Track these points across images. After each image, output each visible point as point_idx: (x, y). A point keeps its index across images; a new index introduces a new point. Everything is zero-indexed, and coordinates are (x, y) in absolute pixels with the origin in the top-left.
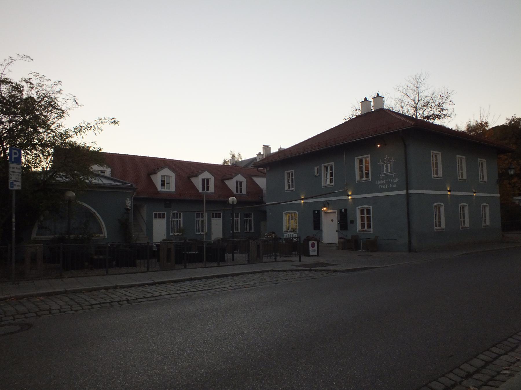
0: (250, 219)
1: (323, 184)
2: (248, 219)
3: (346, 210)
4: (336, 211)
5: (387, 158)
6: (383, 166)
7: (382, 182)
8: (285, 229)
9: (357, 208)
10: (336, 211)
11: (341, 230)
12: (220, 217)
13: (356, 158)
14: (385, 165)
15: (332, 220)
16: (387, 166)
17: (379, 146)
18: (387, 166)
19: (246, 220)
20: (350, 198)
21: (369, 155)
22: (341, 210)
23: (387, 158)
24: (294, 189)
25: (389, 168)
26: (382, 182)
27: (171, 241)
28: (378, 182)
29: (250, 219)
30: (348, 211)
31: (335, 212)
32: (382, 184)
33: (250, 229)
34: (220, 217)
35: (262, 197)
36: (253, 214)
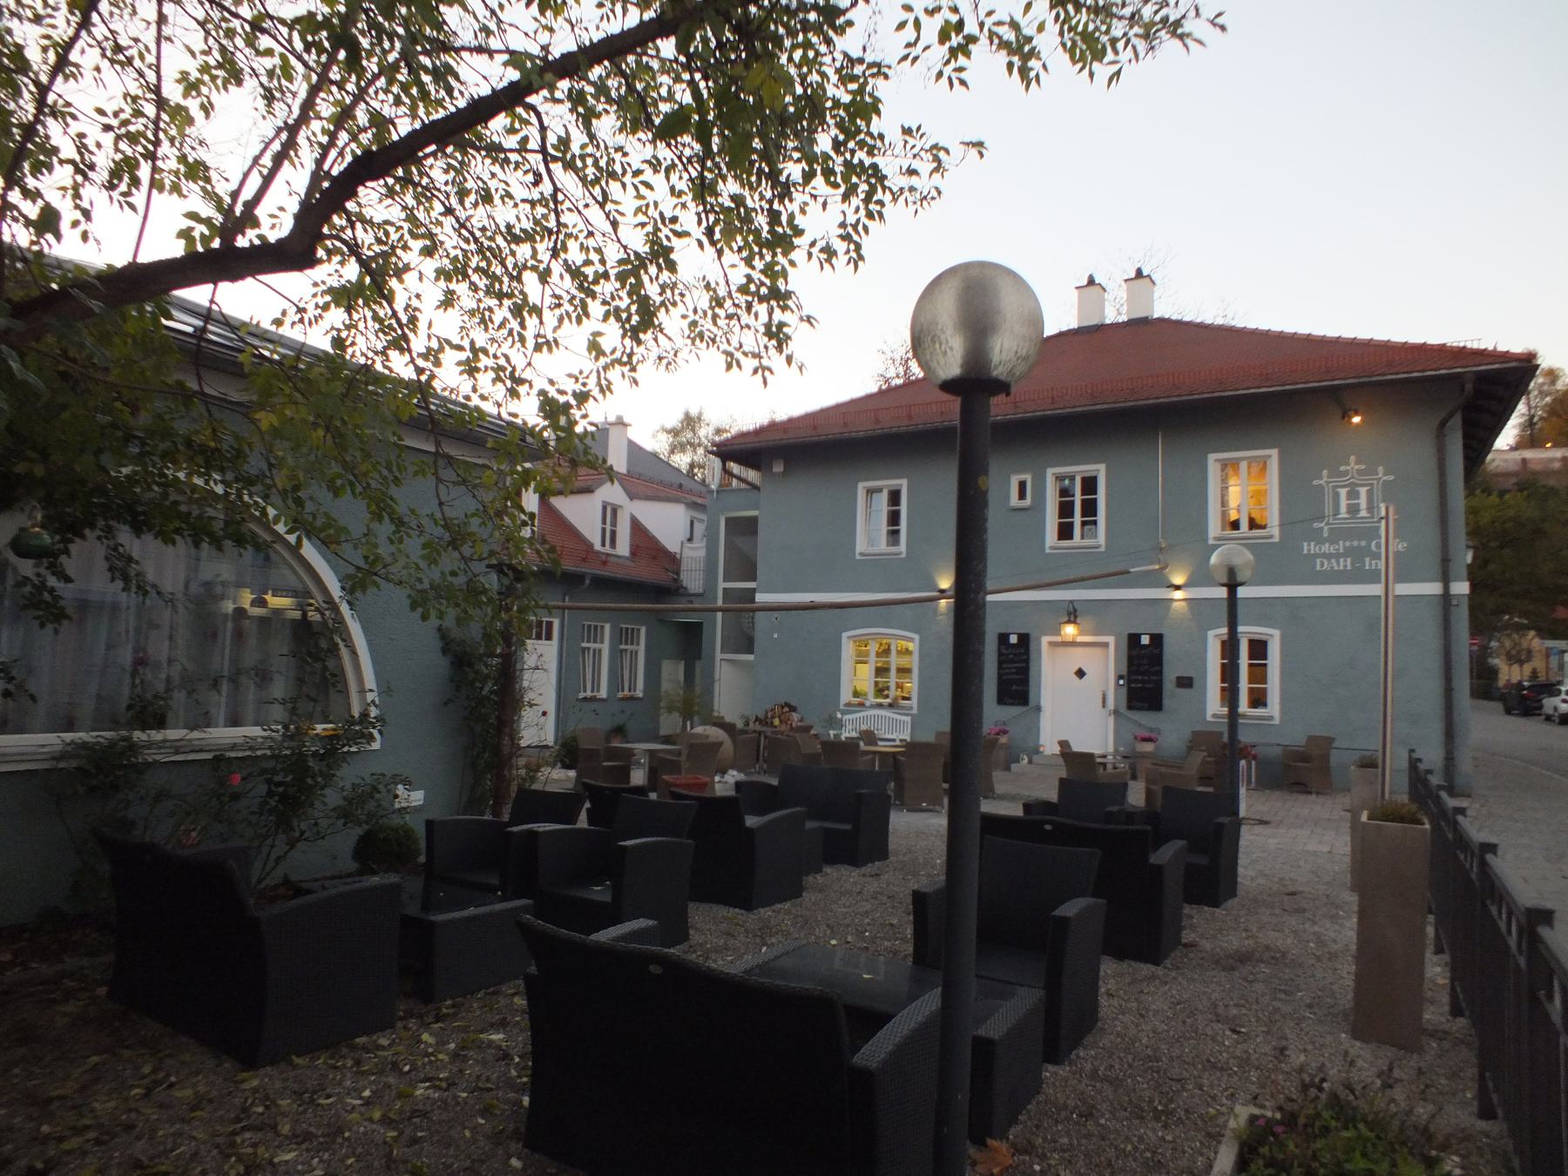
0: (597, 646)
1: (861, 546)
2: (592, 645)
3: (1157, 639)
4: (1111, 640)
5: (1353, 465)
6: (1337, 496)
7: (1326, 548)
8: (846, 696)
9: (845, 635)
10: (1111, 640)
11: (1130, 707)
12: (549, 638)
13: (1212, 457)
14: (1343, 492)
15: (1080, 673)
16: (1353, 495)
17: (1356, 420)
18: (1353, 495)
19: (584, 650)
20: (1178, 595)
21: (1274, 453)
22: (1134, 639)
23: (1353, 465)
24: (1101, 538)
25: (1343, 503)
26: (1326, 548)
27: (1180, 768)
28: (1309, 548)
29: (597, 646)
30: (1167, 642)
31: (1106, 645)
32: (1328, 556)
33: (596, 686)
34: (549, 638)
35: (678, 574)
36: (643, 630)
